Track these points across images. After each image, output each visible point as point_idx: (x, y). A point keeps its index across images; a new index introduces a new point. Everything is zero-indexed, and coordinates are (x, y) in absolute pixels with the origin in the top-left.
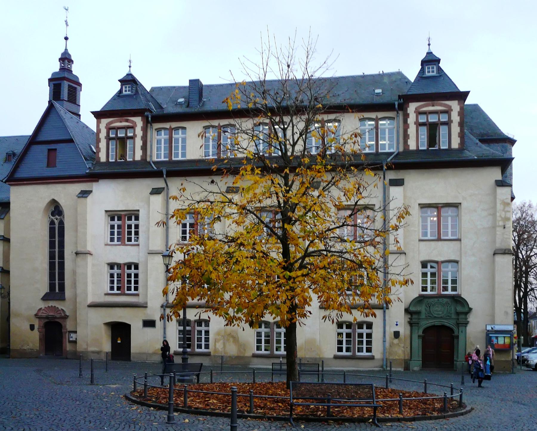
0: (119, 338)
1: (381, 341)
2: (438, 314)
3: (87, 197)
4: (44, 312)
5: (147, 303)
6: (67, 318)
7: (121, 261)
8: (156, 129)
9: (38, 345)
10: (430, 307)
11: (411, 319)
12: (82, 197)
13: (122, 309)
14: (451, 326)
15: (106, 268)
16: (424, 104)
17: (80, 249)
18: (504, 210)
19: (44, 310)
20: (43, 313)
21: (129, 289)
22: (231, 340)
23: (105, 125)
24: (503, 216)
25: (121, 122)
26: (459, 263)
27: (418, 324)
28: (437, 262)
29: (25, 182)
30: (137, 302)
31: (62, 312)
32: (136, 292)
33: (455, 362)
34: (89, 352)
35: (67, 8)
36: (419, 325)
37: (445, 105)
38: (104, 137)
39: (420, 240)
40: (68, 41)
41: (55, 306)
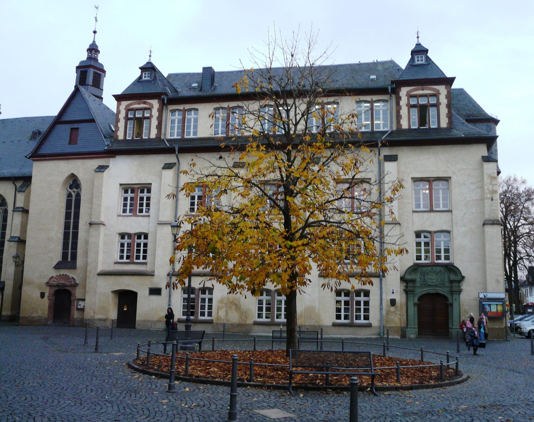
0: (126, 306)
1: (378, 308)
2: (433, 283)
3: (103, 171)
4: (55, 280)
5: (154, 272)
6: (77, 286)
7: (132, 231)
8: (171, 111)
9: (47, 313)
10: (424, 275)
11: (406, 287)
12: (99, 171)
13: (130, 277)
14: (445, 294)
15: (117, 238)
16: (415, 89)
17: (94, 220)
18: (491, 184)
19: (55, 278)
20: (54, 281)
21: (138, 258)
22: (234, 307)
23: (125, 107)
24: (491, 189)
25: (139, 104)
26: (451, 233)
27: (413, 291)
28: (430, 232)
29: (47, 158)
30: (145, 271)
31: (72, 280)
32: (144, 261)
33: (450, 330)
34: (96, 319)
35: (97, 7)
36: (415, 293)
37: (150, 104)
38: (123, 118)
39: (414, 212)
40: (96, 34)
41: (66, 275)
